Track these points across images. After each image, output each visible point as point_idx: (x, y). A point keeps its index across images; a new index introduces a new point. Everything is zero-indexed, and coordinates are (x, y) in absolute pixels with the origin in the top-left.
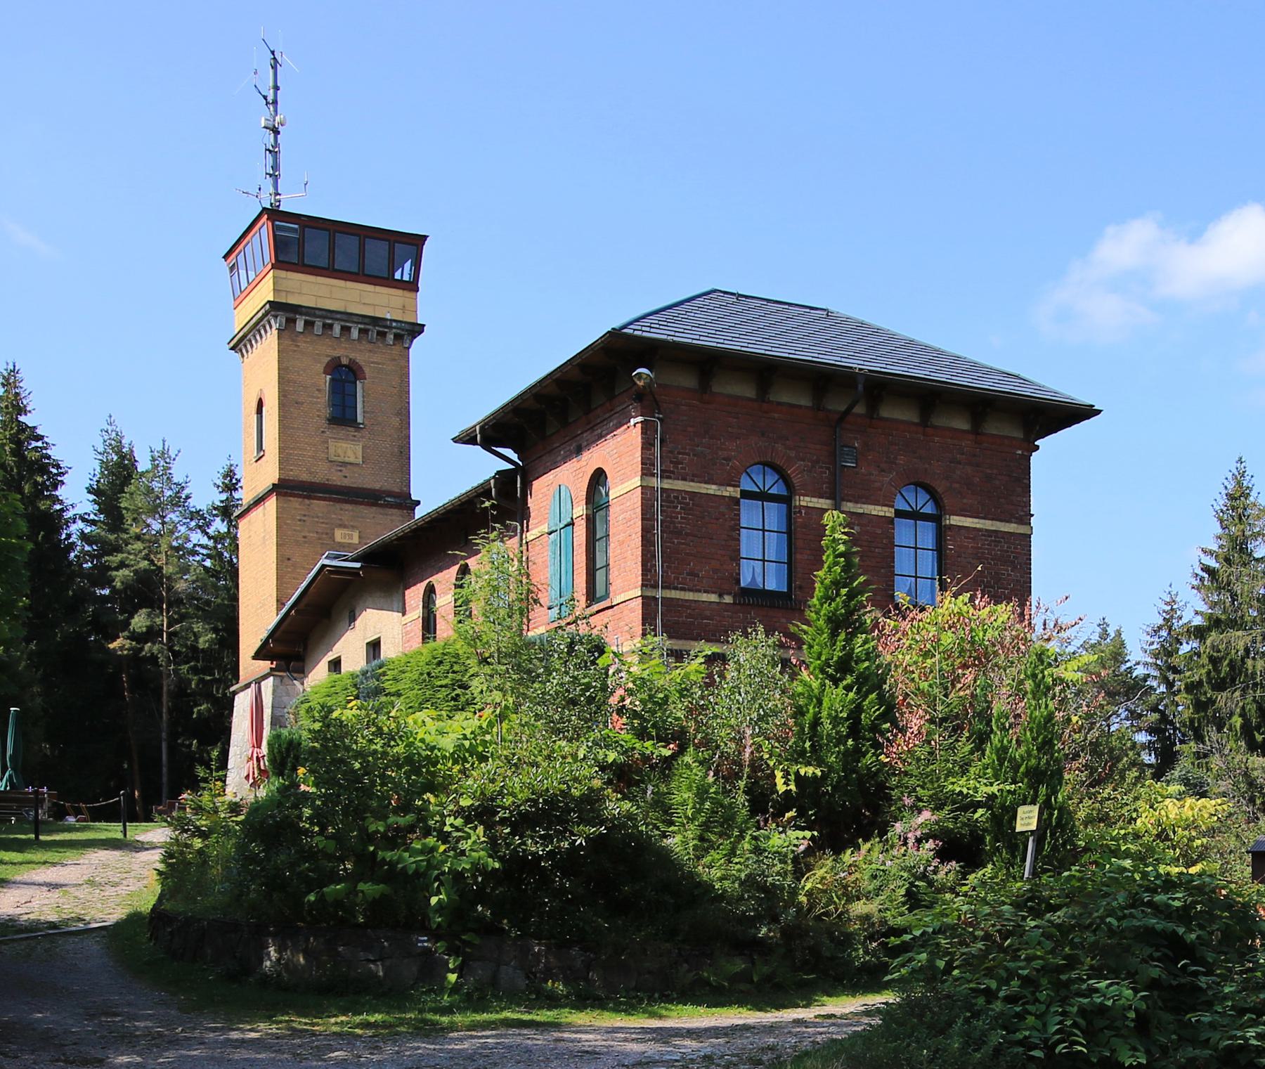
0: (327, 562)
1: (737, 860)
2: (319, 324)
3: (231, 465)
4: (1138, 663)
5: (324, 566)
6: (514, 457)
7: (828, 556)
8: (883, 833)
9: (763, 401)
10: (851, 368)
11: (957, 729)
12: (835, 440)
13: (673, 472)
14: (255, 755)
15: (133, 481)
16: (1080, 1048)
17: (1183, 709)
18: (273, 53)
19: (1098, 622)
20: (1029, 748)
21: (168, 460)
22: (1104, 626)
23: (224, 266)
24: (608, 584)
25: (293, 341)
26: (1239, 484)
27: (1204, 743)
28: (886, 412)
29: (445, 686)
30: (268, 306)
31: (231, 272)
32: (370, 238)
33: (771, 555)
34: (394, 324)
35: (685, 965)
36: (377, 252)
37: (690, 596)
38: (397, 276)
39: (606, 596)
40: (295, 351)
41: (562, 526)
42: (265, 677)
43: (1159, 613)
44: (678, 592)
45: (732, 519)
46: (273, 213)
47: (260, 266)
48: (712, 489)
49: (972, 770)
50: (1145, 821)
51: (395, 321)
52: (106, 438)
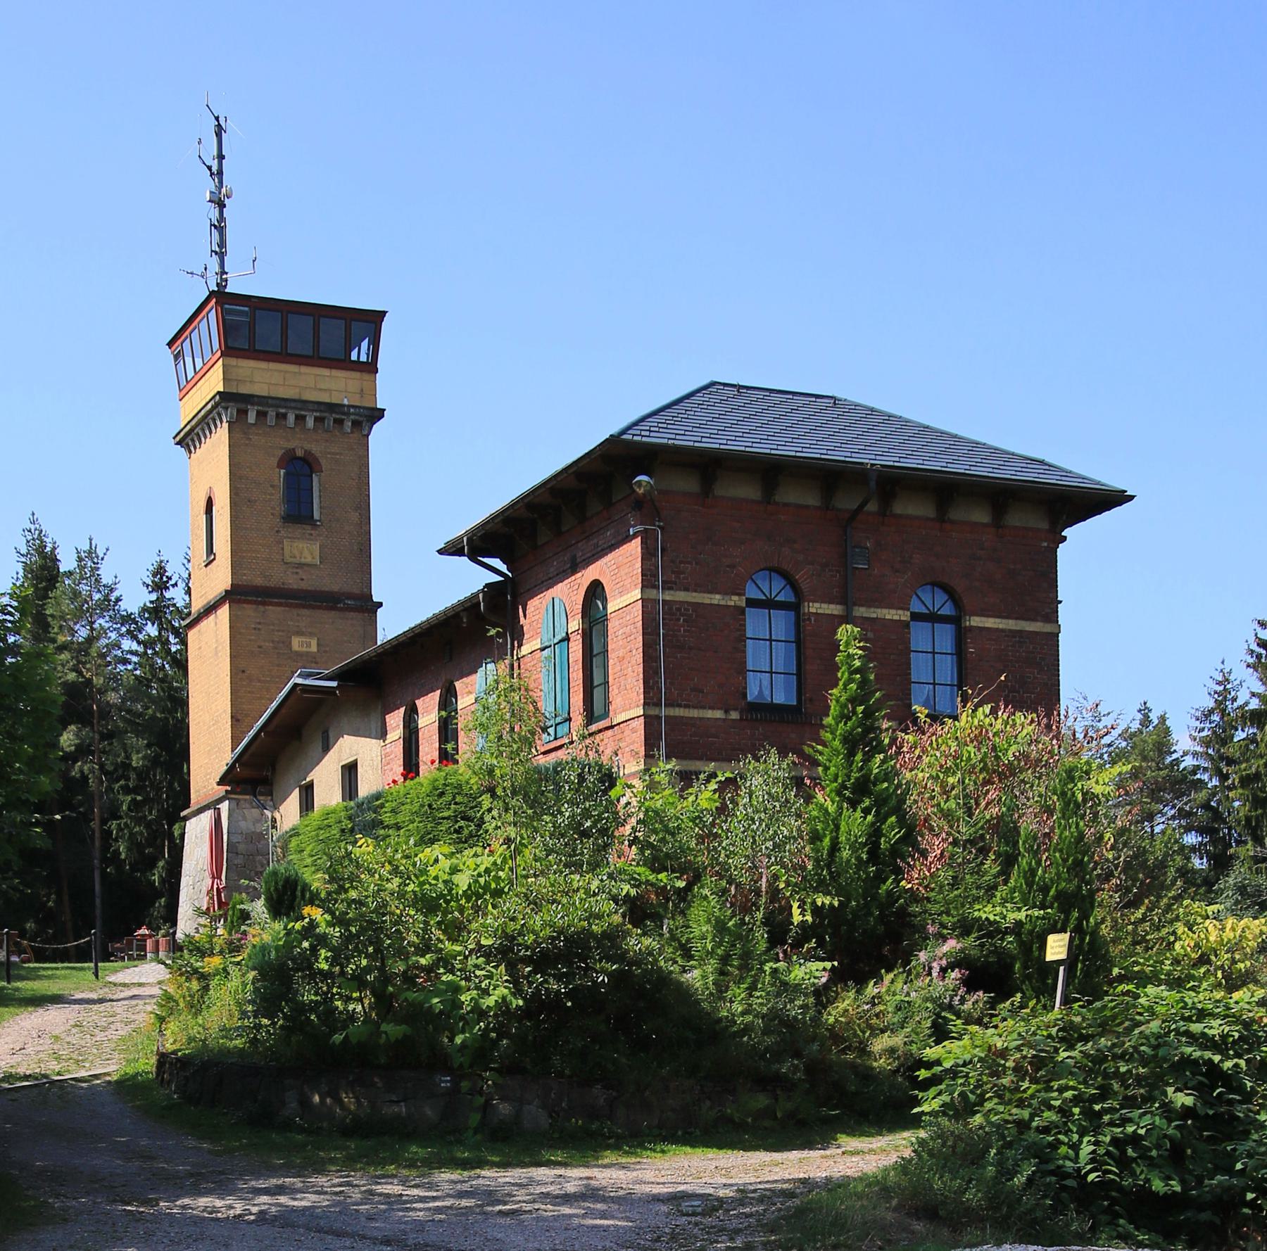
0: (300, 681)
1: (759, 994)
2: (272, 413)
3: (161, 562)
4: (1185, 754)
5: (296, 685)
6: (503, 567)
7: (843, 673)
9: (769, 503)
10: (862, 463)
11: (984, 851)
12: (846, 540)
14: (215, 886)
15: (58, 585)
16: (1112, 1177)
18: (217, 119)
20: (1058, 870)
21: (95, 560)
22: (1145, 711)
23: (168, 354)
25: (245, 433)
28: (899, 508)
30: (218, 397)
31: (175, 361)
32: (324, 316)
33: (779, 666)
34: (352, 410)
35: (708, 1103)
36: (332, 332)
37: (694, 713)
38: (354, 356)
39: (606, 715)
40: (247, 445)
41: (556, 641)
42: (220, 800)
43: (1210, 694)
44: (682, 710)
46: (220, 296)
47: (208, 355)
48: (716, 599)
51: (353, 406)
52: (29, 538)
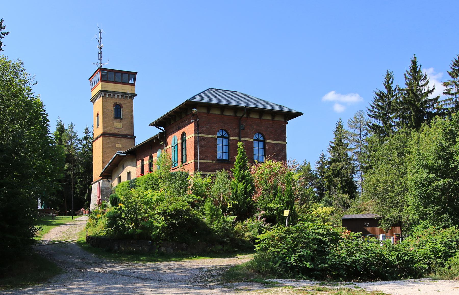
0: (118, 154)
2: (112, 95)
5: (117, 155)
6: (163, 129)
8: (252, 217)
11: (270, 192)
13: (201, 132)
17: (326, 182)
18: (100, 30)
19: (304, 160)
22: (305, 161)
24: (186, 159)
26: (340, 125)
27: (331, 191)
29: (151, 184)
33: (224, 151)
36: (125, 77)
37: (205, 161)
38: (130, 82)
39: (186, 162)
42: (100, 180)
45: (215, 143)
46: (101, 69)
48: (210, 136)
49: (273, 201)
50: (314, 213)
